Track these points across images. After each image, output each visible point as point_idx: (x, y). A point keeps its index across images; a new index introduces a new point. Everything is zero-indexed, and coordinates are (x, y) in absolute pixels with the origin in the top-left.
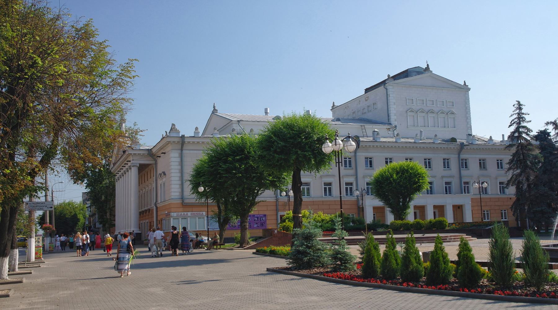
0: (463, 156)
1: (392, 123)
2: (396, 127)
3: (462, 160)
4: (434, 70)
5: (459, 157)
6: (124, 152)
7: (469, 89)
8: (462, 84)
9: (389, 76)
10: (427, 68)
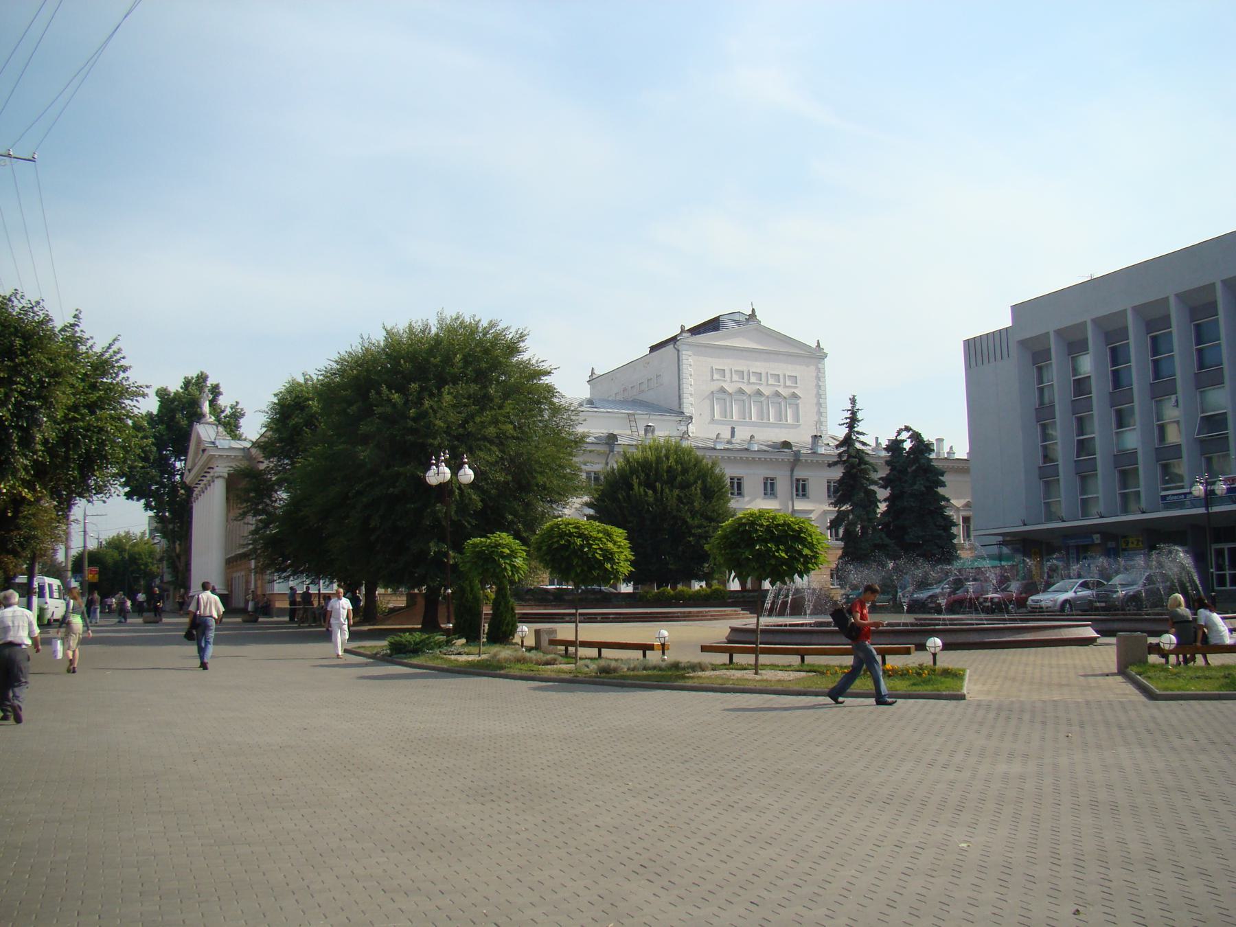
0: (799, 474)
1: (685, 410)
2: (691, 418)
3: (798, 480)
4: (764, 319)
5: (792, 476)
6: (204, 451)
7: (826, 355)
8: (814, 345)
9: (682, 327)
10: (753, 315)
